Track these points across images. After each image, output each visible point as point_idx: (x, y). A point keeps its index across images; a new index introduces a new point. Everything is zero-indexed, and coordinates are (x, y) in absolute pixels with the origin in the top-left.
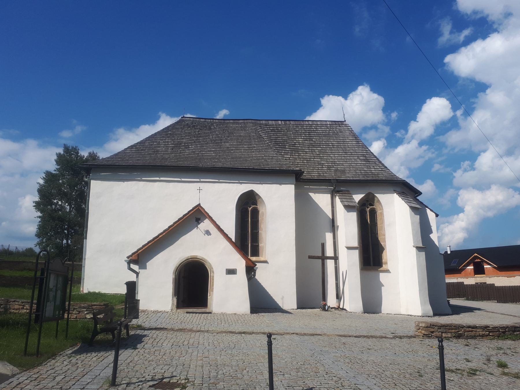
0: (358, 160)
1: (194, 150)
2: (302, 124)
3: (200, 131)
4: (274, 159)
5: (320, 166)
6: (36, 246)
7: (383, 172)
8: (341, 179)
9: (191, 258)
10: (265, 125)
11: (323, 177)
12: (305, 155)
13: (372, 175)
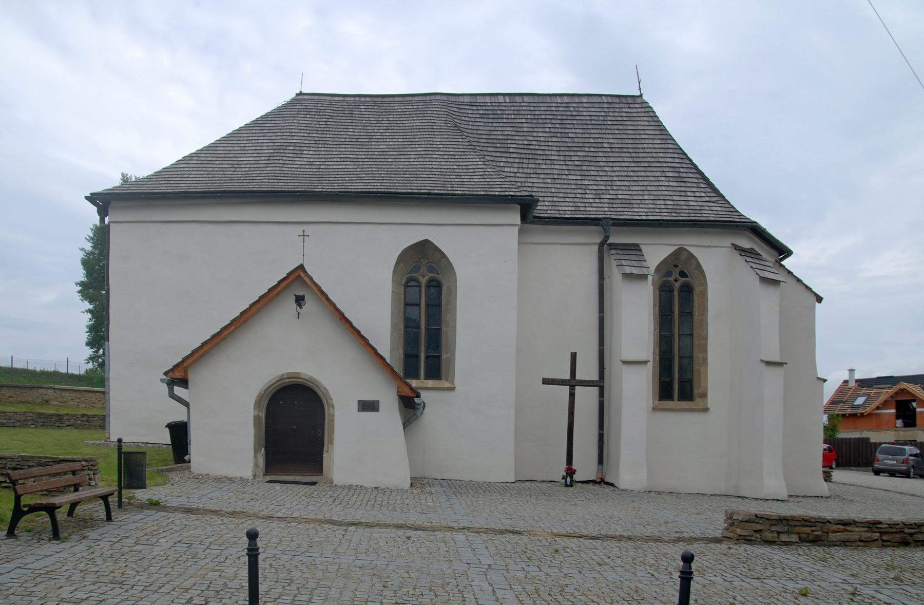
0: (663, 179)
1: (311, 160)
2: (549, 101)
3: (330, 120)
4: (477, 174)
5: (580, 191)
6: (87, 363)
7: (712, 204)
8: (622, 217)
9: (288, 378)
10: (468, 104)
11: (584, 213)
12: (550, 167)
13: (687, 211)
